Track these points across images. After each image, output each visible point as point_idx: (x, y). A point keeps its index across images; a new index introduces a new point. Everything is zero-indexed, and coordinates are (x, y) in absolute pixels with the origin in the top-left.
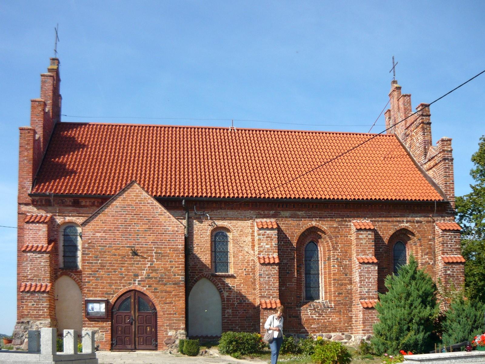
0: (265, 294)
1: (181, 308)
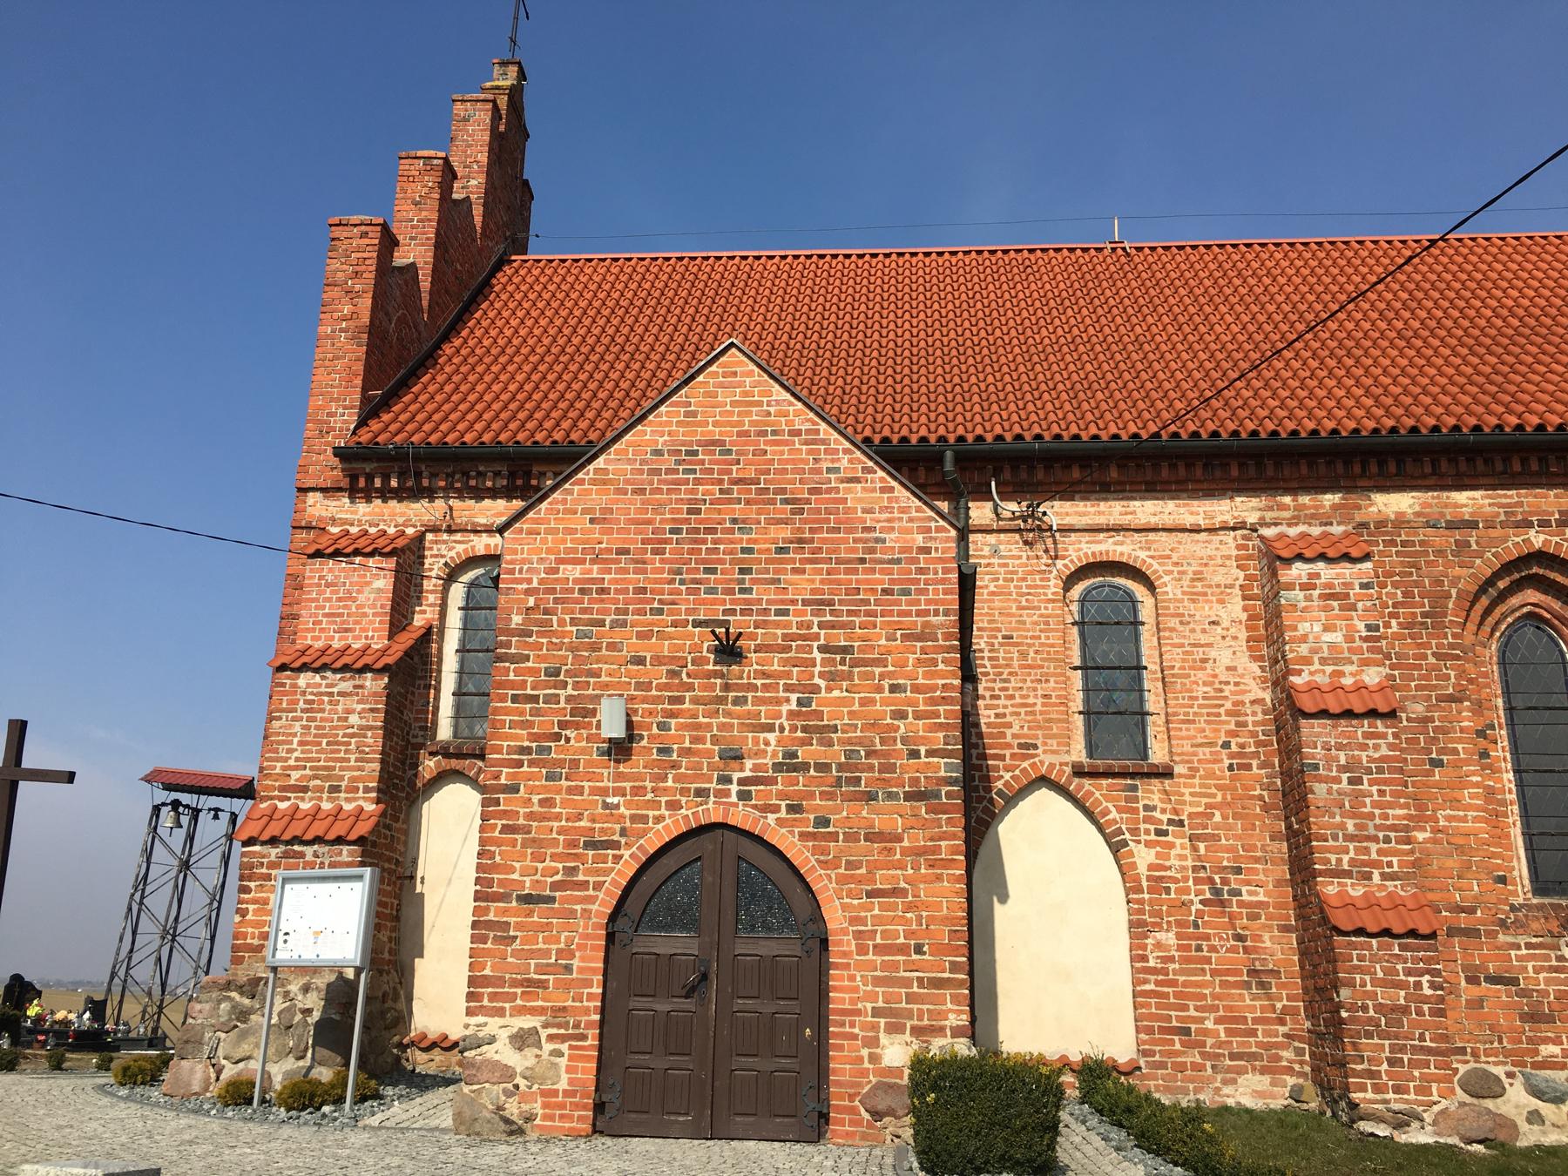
0: (1346, 858)
1: (945, 920)
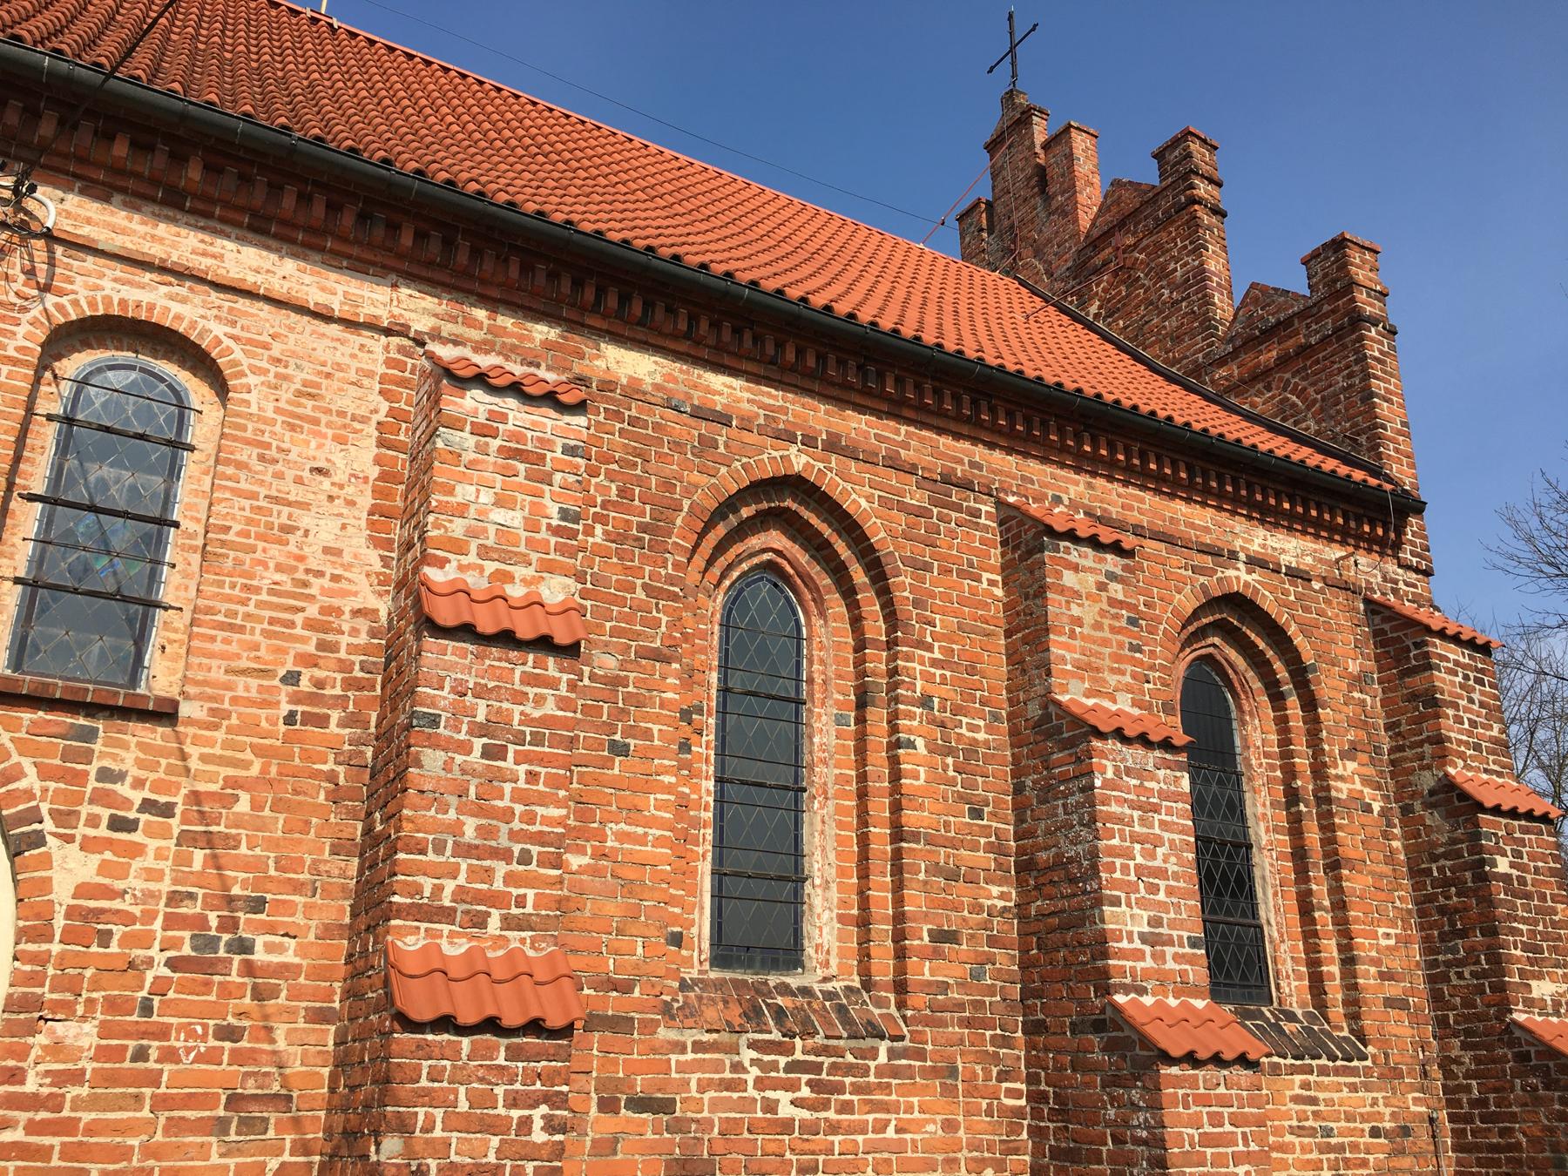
0: (450, 886)
